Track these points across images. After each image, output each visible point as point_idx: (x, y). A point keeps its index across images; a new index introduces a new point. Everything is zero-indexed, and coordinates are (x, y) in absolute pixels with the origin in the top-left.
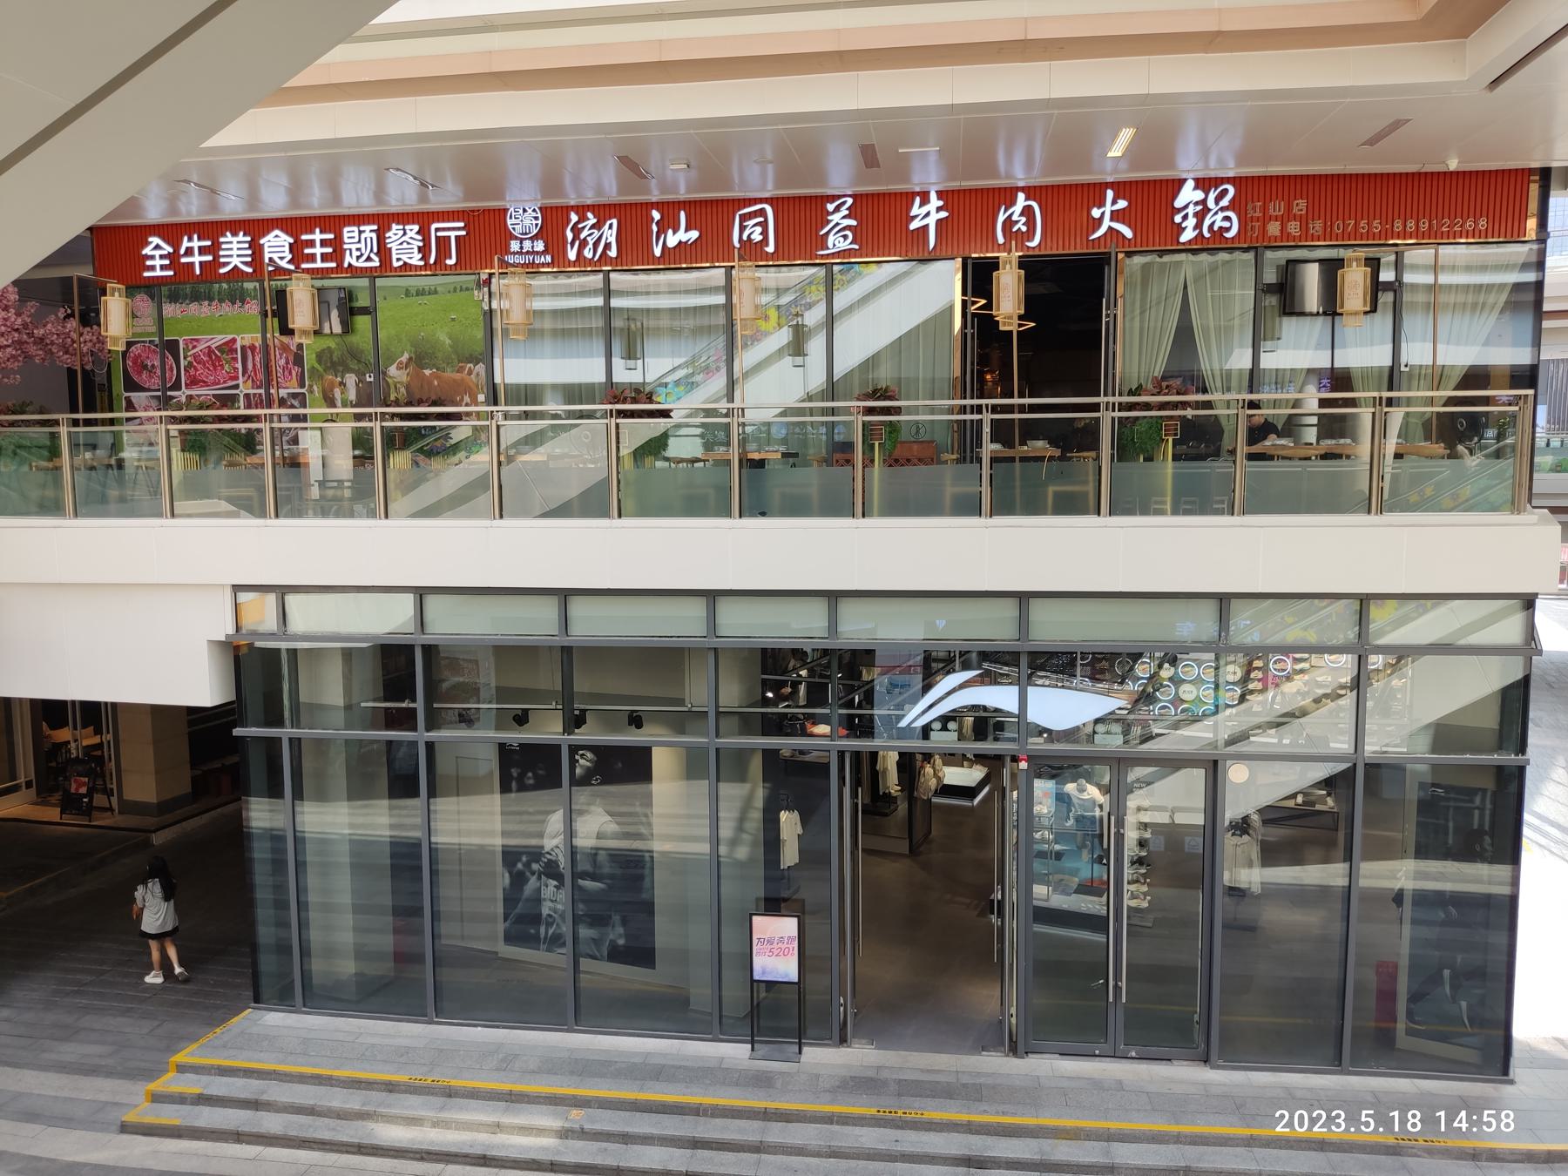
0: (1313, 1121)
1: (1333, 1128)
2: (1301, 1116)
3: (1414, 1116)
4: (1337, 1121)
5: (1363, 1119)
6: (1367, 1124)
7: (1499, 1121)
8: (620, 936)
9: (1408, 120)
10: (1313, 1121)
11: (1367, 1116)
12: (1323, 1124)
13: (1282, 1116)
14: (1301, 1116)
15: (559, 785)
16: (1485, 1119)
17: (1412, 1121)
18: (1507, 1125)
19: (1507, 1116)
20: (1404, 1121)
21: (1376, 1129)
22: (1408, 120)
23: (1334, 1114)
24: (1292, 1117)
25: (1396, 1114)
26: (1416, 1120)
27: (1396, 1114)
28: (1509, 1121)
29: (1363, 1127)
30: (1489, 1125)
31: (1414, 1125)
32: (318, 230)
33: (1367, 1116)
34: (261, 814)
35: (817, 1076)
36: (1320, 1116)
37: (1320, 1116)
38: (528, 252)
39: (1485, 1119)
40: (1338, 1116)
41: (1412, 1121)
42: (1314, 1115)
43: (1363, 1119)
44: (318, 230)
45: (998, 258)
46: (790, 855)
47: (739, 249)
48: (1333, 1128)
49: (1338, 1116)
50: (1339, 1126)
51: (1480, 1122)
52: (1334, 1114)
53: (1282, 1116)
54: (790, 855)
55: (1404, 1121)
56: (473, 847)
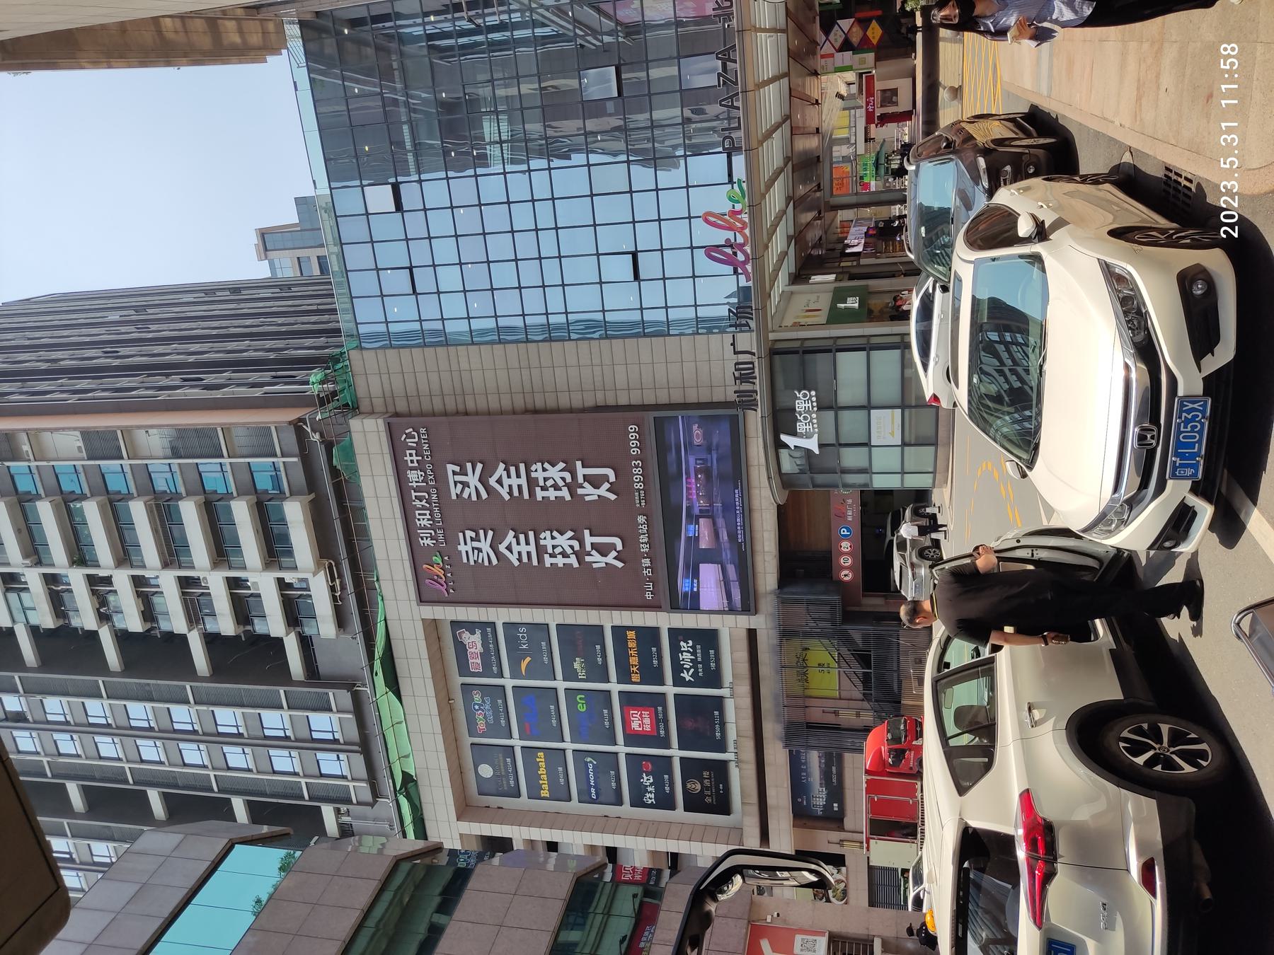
1: (1235, 144)
2: (1226, 217)
4: (1229, 188)
5: (1228, 166)
6: (1232, 163)
7: (1229, 56)
11: (1225, 64)
12: (1232, 199)
13: (1225, 232)
14: (1226, 217)
16: (1228, 67)
17: (1229, 51)
18: (1233, 49)
19: (1225, 49)
21: (1235, 156)
23: (1224, 190)
24: (1226, 224)
25: (1223, 102)
26: (1229, 47)
28: (1229, 47)
29: (1235, 68)
30: (1232, 64)
32: (405, 458)
33: (1225, 64)
37: (1225, 202)
38: (606, 326)
39: (1228, 67)
40: (1225, 140)
41: (1229, 51)
43: (1228, 166)
44: (405, 458)
45: (976, 302)
46: (717, 331)
48: (1235, 144)
50: (1233, 140)
51: (1229, 72)
52: (1224, 190)
53: (1225, 232)
54: (717, 331)
56: (918, 794)
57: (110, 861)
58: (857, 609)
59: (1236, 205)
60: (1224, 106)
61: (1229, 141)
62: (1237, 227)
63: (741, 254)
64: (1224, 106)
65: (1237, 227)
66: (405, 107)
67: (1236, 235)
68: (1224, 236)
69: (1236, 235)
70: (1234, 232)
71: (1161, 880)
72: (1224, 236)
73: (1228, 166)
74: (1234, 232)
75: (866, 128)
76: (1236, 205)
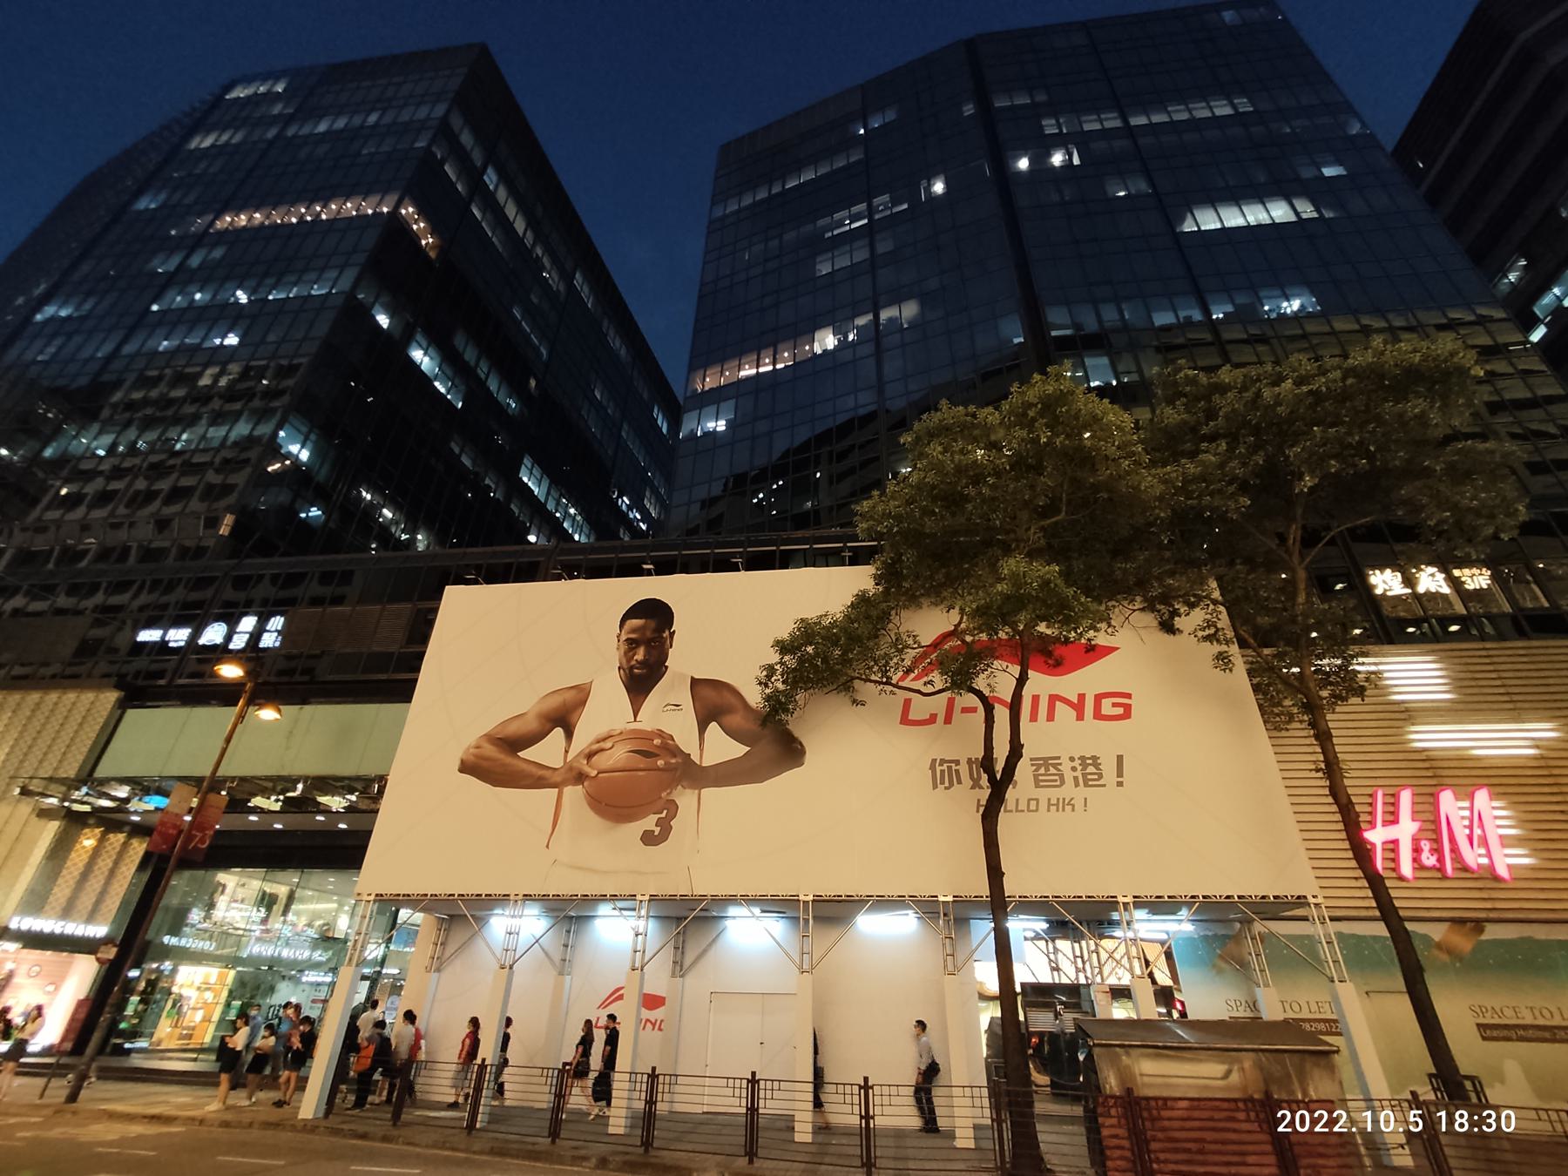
0: (1314, 1122)
1: (1484, 1128)
2: (1302, 1117)
3: (1462, 1116)
4: (1488, 1121)
8: (138, 979)
9: (1118, 648)
10: (1314, 1122)
13: (1284, 1117)
14: (1302, 1117)
15: (1130, 705)
17: (1459, 1121)
19: (1462, 1125)
20: (1451, 1121)
22: (1118, 648)
24: (1293, 1119)
26: (1464, 1121)
27: (1443, 1114)
31: (1462, 1125)
34: (1527, 500)
35: (1325, 1056)
36: (1321, 1116)
37: (1321, 1116)
40: (1489, 1116)
41: (1459, 1121)
42: (1316, 1115)
47: (1067, 575)
48: (1484, 1128)
49: (1489, 1116)
50: (1489, 1126)
53: (1284, 1117)
55: (1451, 1121)
57: (268, 628)
58: (1538, 511)
59: (1317, 1129)
60: (1438, 1114)
61: (1488, 1121)
62: (1290, 1130)
63: (677, 395)
64: (1438, 1114)
65: (1290, 1130)
66: (154, 992)
67: (1280, 1129)
68: (1279, 1115)
69: (1280, 1129)
70: (1285, 1127)
71: (123, 1142)
72: (1279, 1115)
73: (1412, 1119)
74: (1285, 1127)
75: (331, 995)
76: (1317, 1129)
